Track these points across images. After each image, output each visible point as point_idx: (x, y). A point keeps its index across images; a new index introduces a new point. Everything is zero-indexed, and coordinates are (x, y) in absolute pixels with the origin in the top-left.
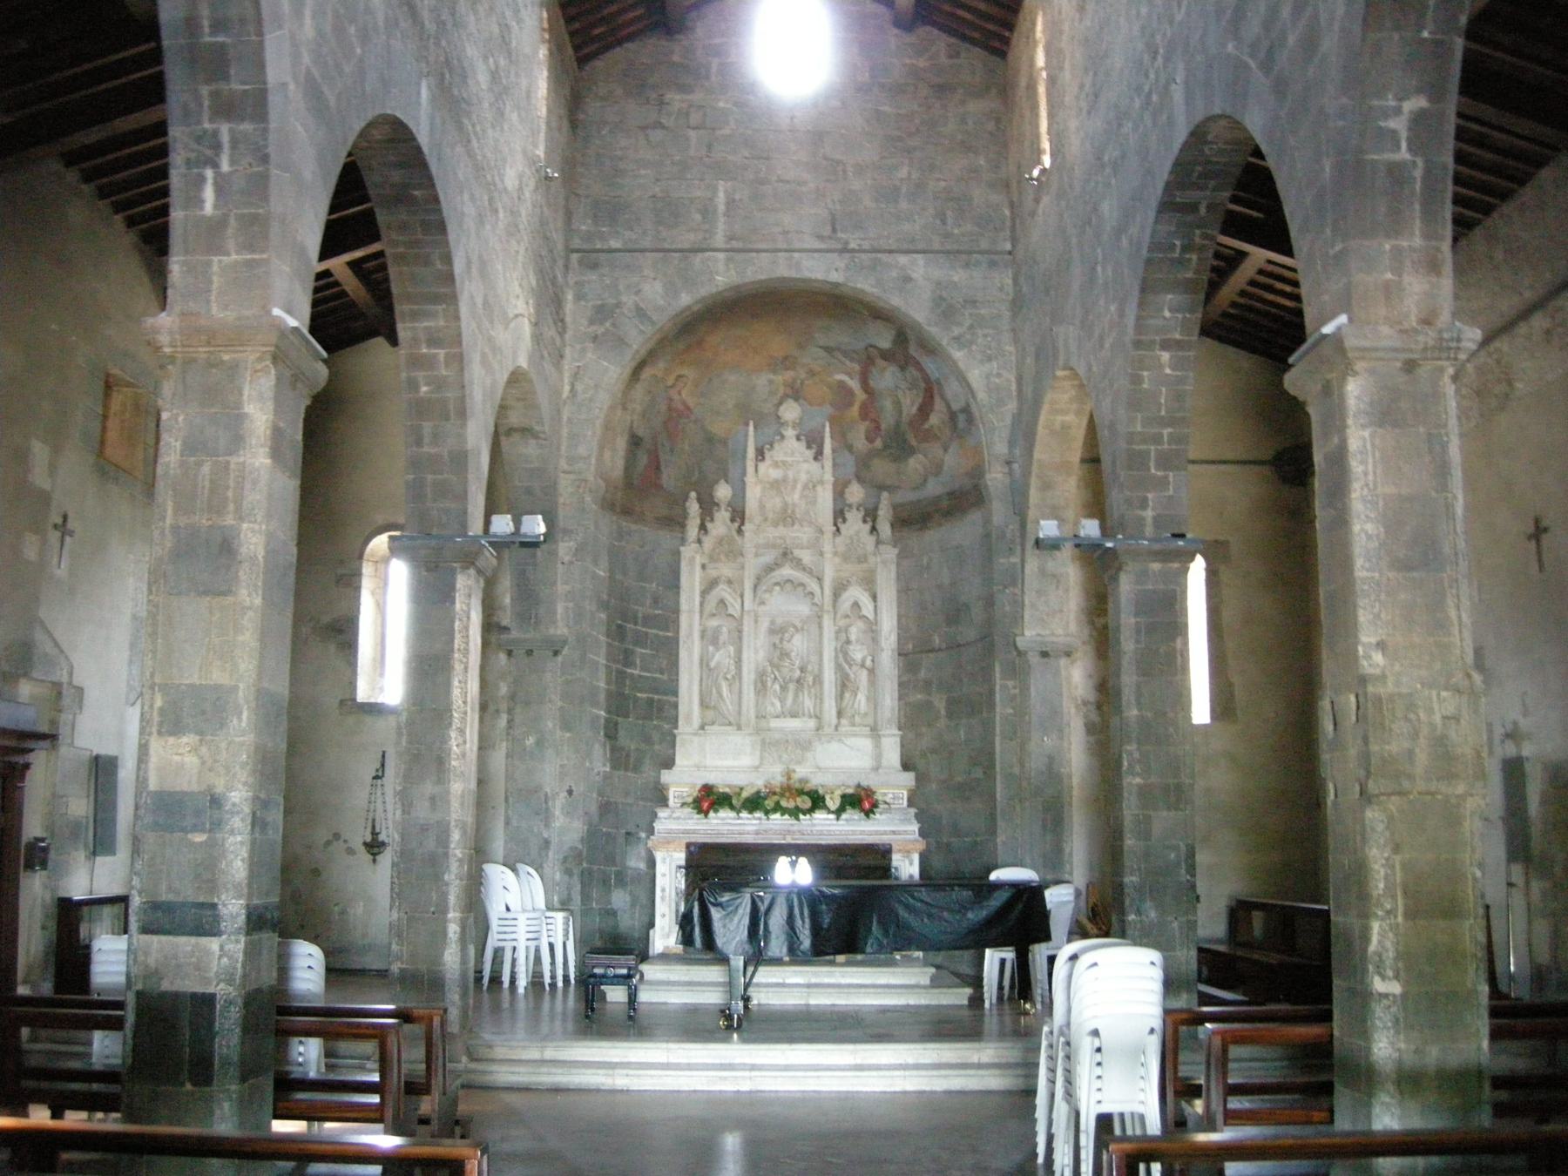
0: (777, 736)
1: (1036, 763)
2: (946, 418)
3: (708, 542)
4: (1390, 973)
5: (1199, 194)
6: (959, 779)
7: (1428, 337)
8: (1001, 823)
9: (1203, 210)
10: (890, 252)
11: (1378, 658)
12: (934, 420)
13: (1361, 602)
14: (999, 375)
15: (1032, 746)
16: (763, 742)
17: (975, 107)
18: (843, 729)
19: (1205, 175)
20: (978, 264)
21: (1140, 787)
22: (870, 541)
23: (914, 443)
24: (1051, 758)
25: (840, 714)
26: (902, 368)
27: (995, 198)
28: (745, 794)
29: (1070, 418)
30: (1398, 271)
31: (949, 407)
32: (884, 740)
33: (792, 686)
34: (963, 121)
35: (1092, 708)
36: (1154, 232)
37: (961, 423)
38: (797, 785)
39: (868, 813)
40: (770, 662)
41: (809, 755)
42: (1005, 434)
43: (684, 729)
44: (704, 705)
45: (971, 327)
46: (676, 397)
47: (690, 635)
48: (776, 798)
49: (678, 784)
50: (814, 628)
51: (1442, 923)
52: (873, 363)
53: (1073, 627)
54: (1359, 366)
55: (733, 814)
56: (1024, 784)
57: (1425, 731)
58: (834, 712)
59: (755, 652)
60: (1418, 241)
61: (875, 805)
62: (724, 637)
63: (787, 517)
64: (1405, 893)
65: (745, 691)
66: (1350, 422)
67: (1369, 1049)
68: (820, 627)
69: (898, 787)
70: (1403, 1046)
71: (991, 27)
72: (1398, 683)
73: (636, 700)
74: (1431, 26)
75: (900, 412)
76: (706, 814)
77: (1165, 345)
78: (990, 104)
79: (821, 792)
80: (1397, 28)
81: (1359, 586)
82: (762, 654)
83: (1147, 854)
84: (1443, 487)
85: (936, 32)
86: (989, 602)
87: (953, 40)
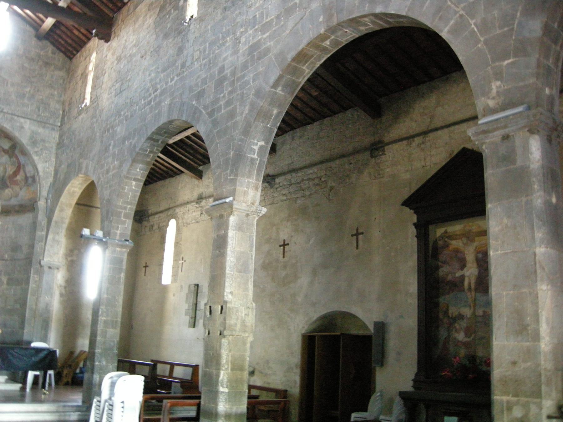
1: (42, 305)
2: (24, 178)
4: (225, 386)
5: (161, 137)
6: (9, 307)
7: (254, 209)
8: (26, 325)
9: (160, 142)
10: (18, 116)
11: (230, 296)
12: (19, 178)
13: (227, 280)
14: (48, 168)
15: (41, 299)
17: (57, 73)
19: (166, 133)
20: (48, 128)
21: (105, 321)
23: (9, 184)
24: (47, 304)
26: (10, 157)
27: (57, 106)
29: (76, 190)
30: (248, 188)
31: (26, 175)
34: (52, 77)
35: (63, 288)
36: (143, 145)
37: (30, 181)
42: (47, 188)
45: (42, 149)
51: (239, 372)
53: (61, 259)
54: (235, 213)
56: (37, 312)
57: (240, 318)
60: (254, 181)
64: (231, 363)
66: (230, 228)
67: (216, 408)
70: (227, 407)
71: (70, 48)
72: (235, 304)
74: (270, 124)
75: (5, 172)
77: (135, 180)
78: (62, 73)
80: (263, 122)
81: (227, 275)
83: (104, 343)
84: (251, 251)
85: (49, 44)
86: (32, 246)
87: (54, 48)
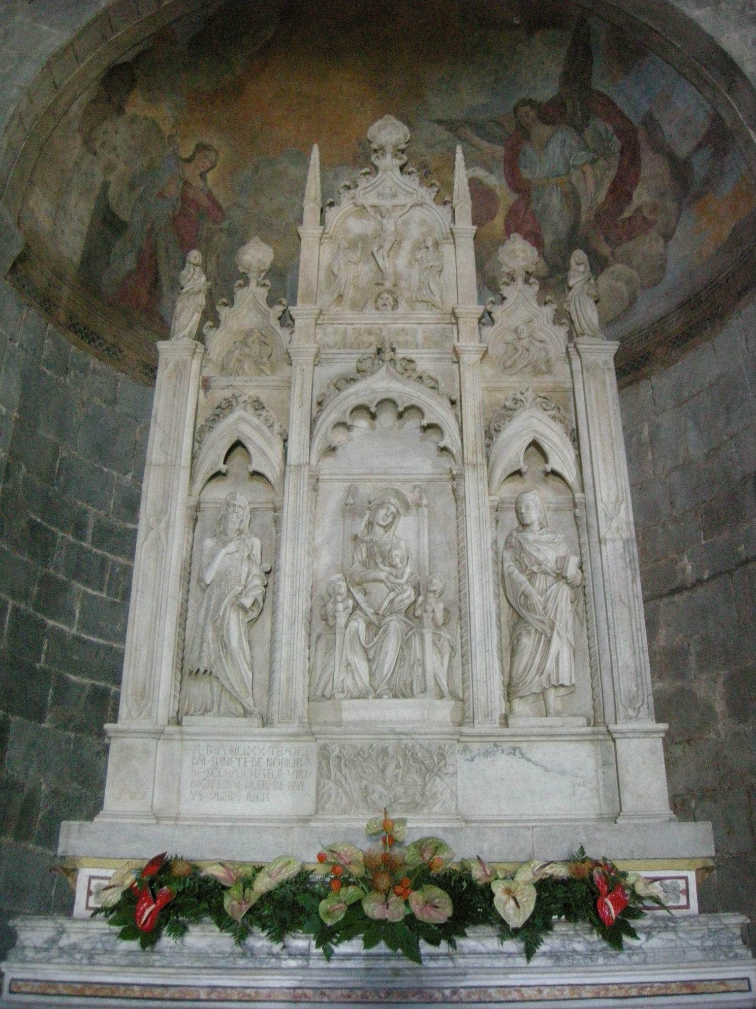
0: (360, 741)
3: (218, 341)
16: (324, 754)
18: (518, 723)
22: (555, 338)
25: (510, 690)
28: (263, 884)
32: (623, 745)
33: (395, 624)
38: (411, 857)
39: (615, 933)
40: (349, 578)
41: (439, 785)
43: (130, 721)
44: (187, 670)
46: (197, 182)
47: (163, 512)
48: (351, 893)
49: (102, 859)
50: (444, 502)
52: (527, 137)
55: (225, 941)
58: (498, 691)
59: (311, 553)
61: (632, 908)
62: (238, 519)
63: (383, 293)
65: (283, 636)
68: (457, 497)
69: (674, 860)
73: (63, 686)
76: (149, 938)
79: (477, 873)
82: (325, 559)
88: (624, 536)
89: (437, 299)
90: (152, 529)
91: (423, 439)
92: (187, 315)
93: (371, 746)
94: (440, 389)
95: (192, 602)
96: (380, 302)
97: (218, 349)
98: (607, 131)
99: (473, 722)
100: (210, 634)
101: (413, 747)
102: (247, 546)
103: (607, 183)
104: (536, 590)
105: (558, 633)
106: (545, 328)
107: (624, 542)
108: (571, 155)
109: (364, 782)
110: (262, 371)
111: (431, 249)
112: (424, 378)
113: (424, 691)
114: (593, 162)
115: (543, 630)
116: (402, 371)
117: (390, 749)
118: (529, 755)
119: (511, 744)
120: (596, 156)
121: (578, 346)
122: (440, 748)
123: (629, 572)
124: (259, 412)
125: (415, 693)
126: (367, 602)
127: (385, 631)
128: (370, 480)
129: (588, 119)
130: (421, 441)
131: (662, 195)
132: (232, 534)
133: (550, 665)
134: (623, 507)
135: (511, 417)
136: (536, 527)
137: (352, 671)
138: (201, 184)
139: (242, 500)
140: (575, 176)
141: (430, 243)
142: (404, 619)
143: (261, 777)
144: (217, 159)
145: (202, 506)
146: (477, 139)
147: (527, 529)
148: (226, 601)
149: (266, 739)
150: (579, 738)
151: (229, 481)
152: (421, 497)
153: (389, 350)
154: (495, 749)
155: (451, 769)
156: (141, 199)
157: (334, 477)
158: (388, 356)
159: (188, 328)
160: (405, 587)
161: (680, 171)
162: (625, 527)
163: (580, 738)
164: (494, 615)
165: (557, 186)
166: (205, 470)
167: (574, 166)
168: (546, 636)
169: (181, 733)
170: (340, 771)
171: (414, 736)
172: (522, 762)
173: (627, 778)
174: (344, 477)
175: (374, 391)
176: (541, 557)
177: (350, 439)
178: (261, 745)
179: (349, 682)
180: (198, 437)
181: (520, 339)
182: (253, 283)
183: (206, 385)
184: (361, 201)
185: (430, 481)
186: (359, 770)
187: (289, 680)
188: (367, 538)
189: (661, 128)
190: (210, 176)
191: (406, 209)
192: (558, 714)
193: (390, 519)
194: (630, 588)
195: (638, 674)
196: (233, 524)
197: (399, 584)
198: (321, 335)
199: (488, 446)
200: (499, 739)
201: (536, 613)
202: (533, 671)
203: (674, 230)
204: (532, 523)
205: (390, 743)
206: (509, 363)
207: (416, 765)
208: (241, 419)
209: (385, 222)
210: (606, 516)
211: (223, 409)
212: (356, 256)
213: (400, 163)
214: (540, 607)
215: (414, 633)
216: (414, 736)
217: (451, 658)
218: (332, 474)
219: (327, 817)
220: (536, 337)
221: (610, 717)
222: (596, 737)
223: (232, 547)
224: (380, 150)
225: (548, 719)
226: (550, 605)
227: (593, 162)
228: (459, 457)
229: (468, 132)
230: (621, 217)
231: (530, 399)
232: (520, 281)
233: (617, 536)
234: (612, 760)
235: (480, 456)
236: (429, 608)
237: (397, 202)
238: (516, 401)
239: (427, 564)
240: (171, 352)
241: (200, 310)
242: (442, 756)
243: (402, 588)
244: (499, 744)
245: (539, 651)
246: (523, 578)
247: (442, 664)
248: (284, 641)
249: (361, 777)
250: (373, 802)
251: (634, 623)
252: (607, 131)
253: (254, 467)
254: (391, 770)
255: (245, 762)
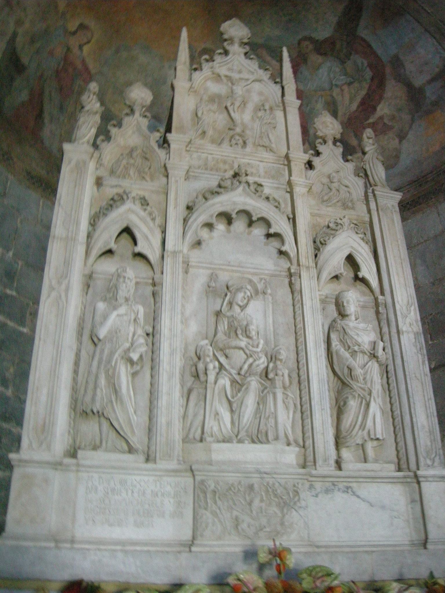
0: (232, 478)
22: (357, 186)
41: (294, 516)
44: (81, 411)
46: (76, 50)
47: (64, 275)
52: (305, 61)
59: (183, 323)
62: (126, 289)
82: (193, 328)
88: (415, 330)
89: (273, 146)
90: (54, 289)
91: (266, 244)
92: (87, 127)
93: (240, 483)
94: (281, 209)
95: (83, 353)
96: (233, 142)
97: (108, 158)
98: (362, 63)
99: (315, 465)
100: (102, 381)
101: (274, 484)
102: (134, 311)
103: (359, 99)
104: (357, 363)
105: (374, 398)
106: (349, 178)
107: (415, 334)
108: (335, 78)
109: (235, 513)
110: (143, 178)
111: (268, 112)
112: (270, 199)
113: (277, 438)
114: (350, 84)
115: (364, 396)
116: (253, 190)
117: (256, 486)
118: (359, 493)
119: (345, 484)
120: (352, 80)
121: (376, 192)
122: (294, 486)
123: (420, 355)
124: (145, 207)
125: (270, 440)
126: (229, 364)
127: (247, 388)
128: (227, 271)
129: (351, 54)
130: (265, 245)
131: (399, 110)
132: (121, 300)
133: (369, 423)
134: (412, 308)
135: (334, 236)
136: (353, 318)
137: (218, 420)
138: (78, 53)
139: (130, 273)
140: (336, 92)
141: (267, 107)
142: (260, 380)
143: (147, 506)
144: (92, 38)
145: (93, 275)
146: (269, 58)
147: (347, 318)
148: (117, 355)
149: (151, 473)
150: (392, 480)
151: (116, 258)
152: (266, 287)
153: (244, 175)
154: (333, 487)
155: (303, 503)
156: (38, 52)
157: (201, 265)
158: (243, 179)
159: (87, 138)
160: (260, 355)
161: (415, 95)
162: (415, 323)
163: (395, 480)
164: (326, 382)
165: (322, 96)
166: (98, 248)
167: (336, 86)
168: (366, 400)
169: (78, 465)
170: (215, 503)
171: (275, 476)
172: (354, 498)
173: (430, 512)
174: (209, 266)
175: (234, 203)
176: (360, 340)
177: (212, 238)
178: (146, 478)
179: (216, 429)
180: (93, 223)
181: (332, 182)
182: (137, 114)
183: (99, 182)
184: (217, 70)
185: (272, 276)
186: (231, 502)
187: (169, 424)
188: (229, 314)
189: (404, 66)
190: (86, 48)
191: (249, 82)
192: (376, 461)
193: (245, 301)
194: (421, 368)
195: (431, 432)
196: (122, 293)
197: (255, 352)
198: (190, 159)
199: (316, 256)
200: (338, 480)
201: (358, 382)
202: (357, 427)
203: (407, 134)
204: (351, 315)
205: (255, 480)
206: (326, 198)
207: (276, 500)
208: (130, 210)
209: (234, 87)
210: (402, 314)
211: (115, 202)
212: (215, 107)
213: (244, 51)
214: (362, 378)
215: (268, 392)
216: (275, 476)
217: (294, 412)
218: (199, 262)
219: (206, 543)
220: (343, 183)
221: (413, 466)
222: (405, 480)
223: (122, 310)
224: (231, 40)
225: (366, 464)
226: (368, 377)
227: (350, 84)
228: (295, 261)
229: (264, 53)
230: (368, 122)
231: (347, 224)
232: (330, 143)
233: (410, 329)
234: (417, 498)
235: (310, 261)
236: (280, 373)
237: (242, 76)
238: (337, 224)
239: (272, 339)
240: (75, 153)
241: (97, 126)
242: (296, 493)
243: (258, 356)
244: (336, 483)
245: (362, 412)
246: (347, 355)
247: (288, 418)
248: (164, 391)
249: (232, 508)
250: (243, 529)
251: (426, 395)
252: (362, 63)
253: (138, 249)
254: (256, 503)
255: (133, 492)
